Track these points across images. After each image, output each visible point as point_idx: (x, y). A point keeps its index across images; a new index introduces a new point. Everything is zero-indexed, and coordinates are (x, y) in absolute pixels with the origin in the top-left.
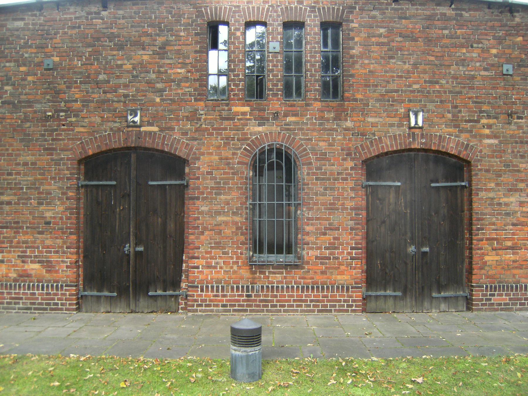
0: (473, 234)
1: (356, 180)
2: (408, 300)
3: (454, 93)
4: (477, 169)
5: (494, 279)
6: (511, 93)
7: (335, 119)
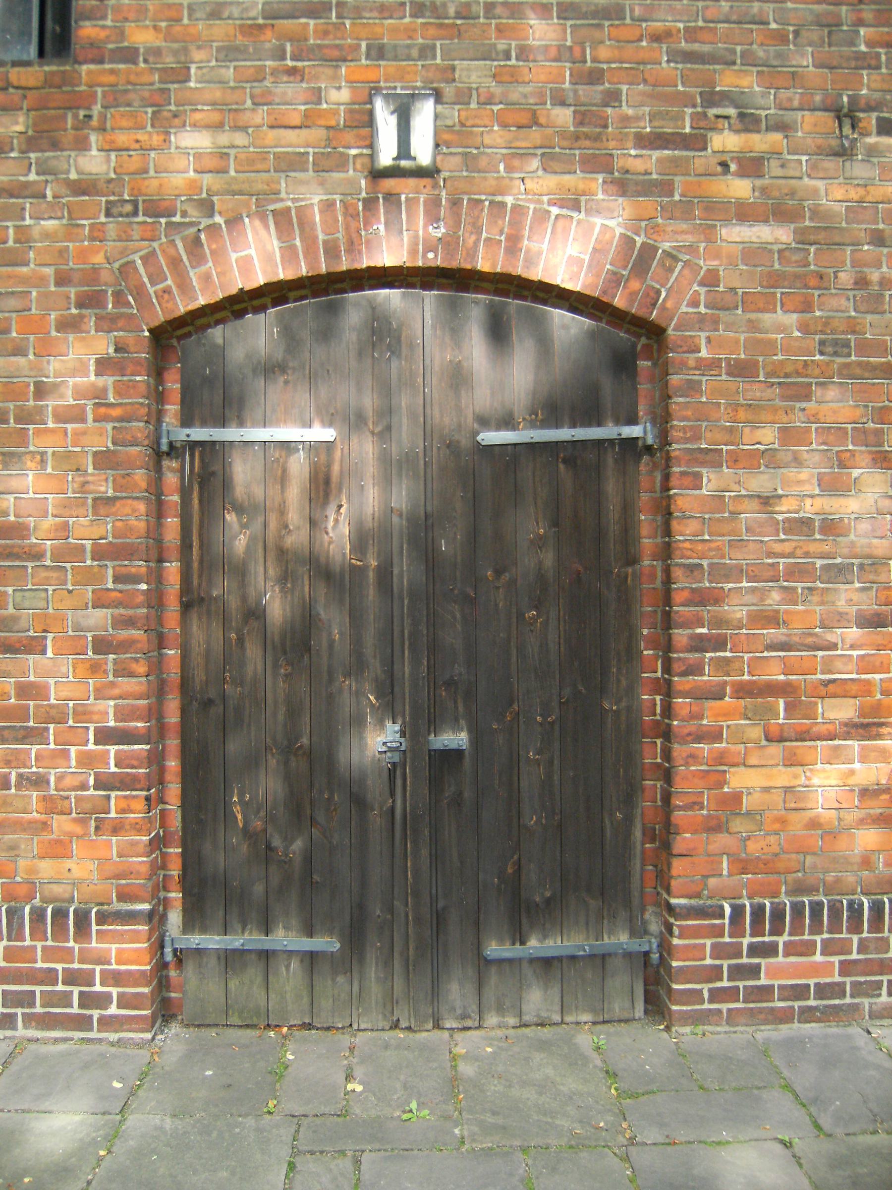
0: (677, 667)
1: (121, 419)
2: (373, 971)
3: (584, 16)
4: (692, 363)
5: (772, 877)
6: (852, 17)
7: (31, 143)
